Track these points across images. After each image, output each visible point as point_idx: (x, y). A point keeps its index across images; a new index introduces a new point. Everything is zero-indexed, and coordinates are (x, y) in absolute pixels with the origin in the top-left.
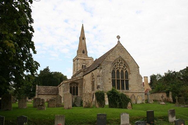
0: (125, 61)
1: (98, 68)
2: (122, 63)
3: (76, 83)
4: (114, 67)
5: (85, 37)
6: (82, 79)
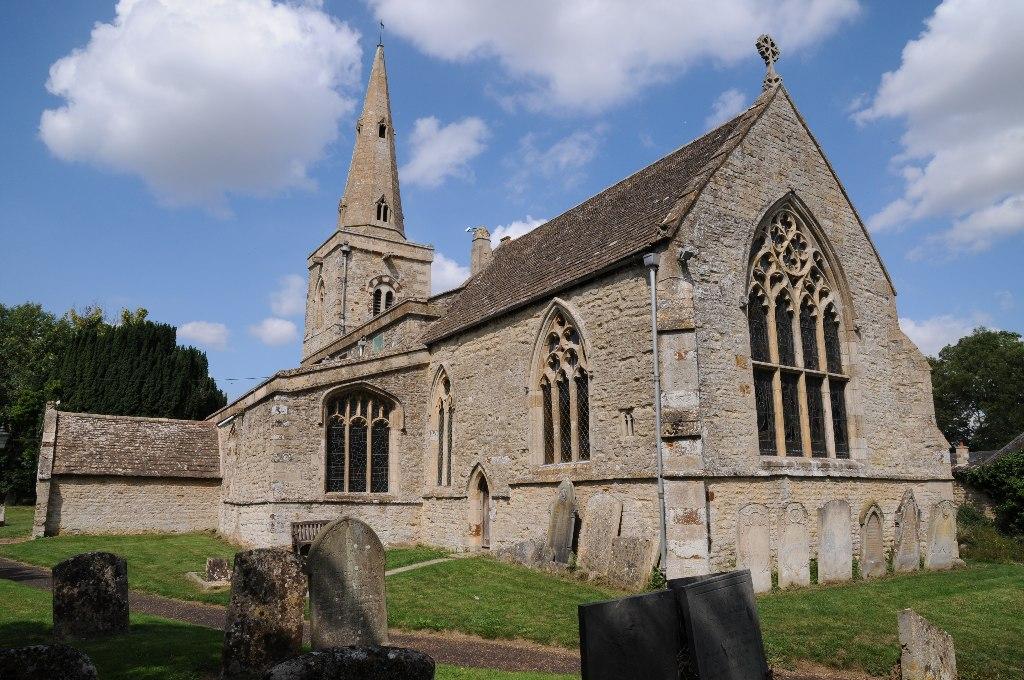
2: (800, 245)
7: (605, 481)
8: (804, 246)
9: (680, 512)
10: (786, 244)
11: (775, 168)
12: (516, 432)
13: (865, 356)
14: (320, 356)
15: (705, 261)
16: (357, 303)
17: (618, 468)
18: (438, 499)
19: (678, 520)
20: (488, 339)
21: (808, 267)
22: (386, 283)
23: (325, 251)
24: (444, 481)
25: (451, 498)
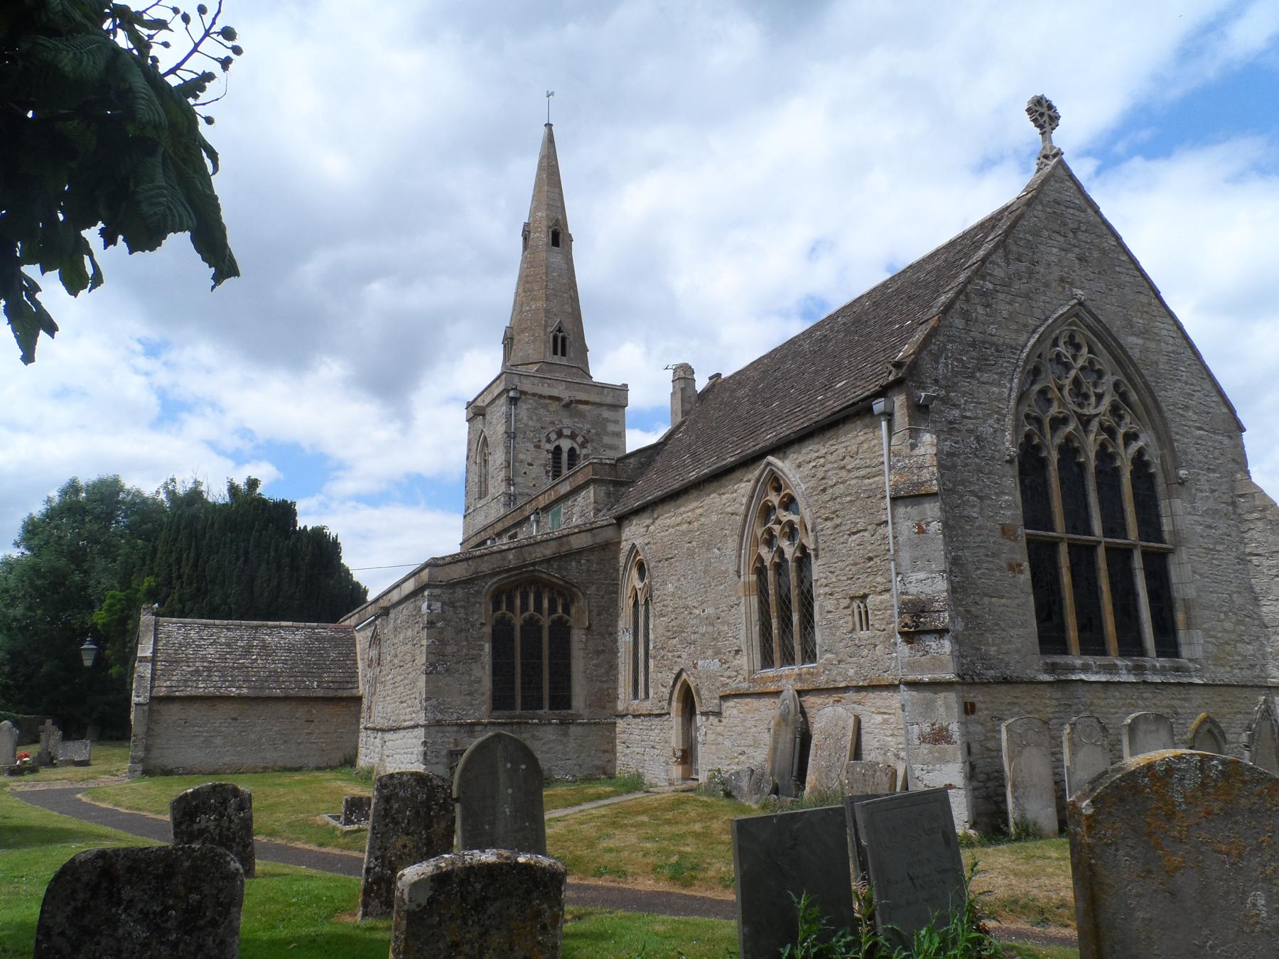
0: (1122, 359)
1: (879, 406)
3: (549, 585)
4: (1036, 412)
5: (572, 229)
6: (611, 547)
7: (837, 690)
8: (1100, 374)
9: (926, 728)
10: (1073, 373)
11: (1056, 273)
12: (726, 628)
13: (1196, 518)
14: (483, 536)
15: (954, 405)
16: (530, 464)
17: (851, 672)
18: (634, 716)
19: (923, 739)
20: (691, 509)
21: (1106, 401)
22: (567, 437)
23: (488, 399)
24: (641, 694)
25: (650, 715)
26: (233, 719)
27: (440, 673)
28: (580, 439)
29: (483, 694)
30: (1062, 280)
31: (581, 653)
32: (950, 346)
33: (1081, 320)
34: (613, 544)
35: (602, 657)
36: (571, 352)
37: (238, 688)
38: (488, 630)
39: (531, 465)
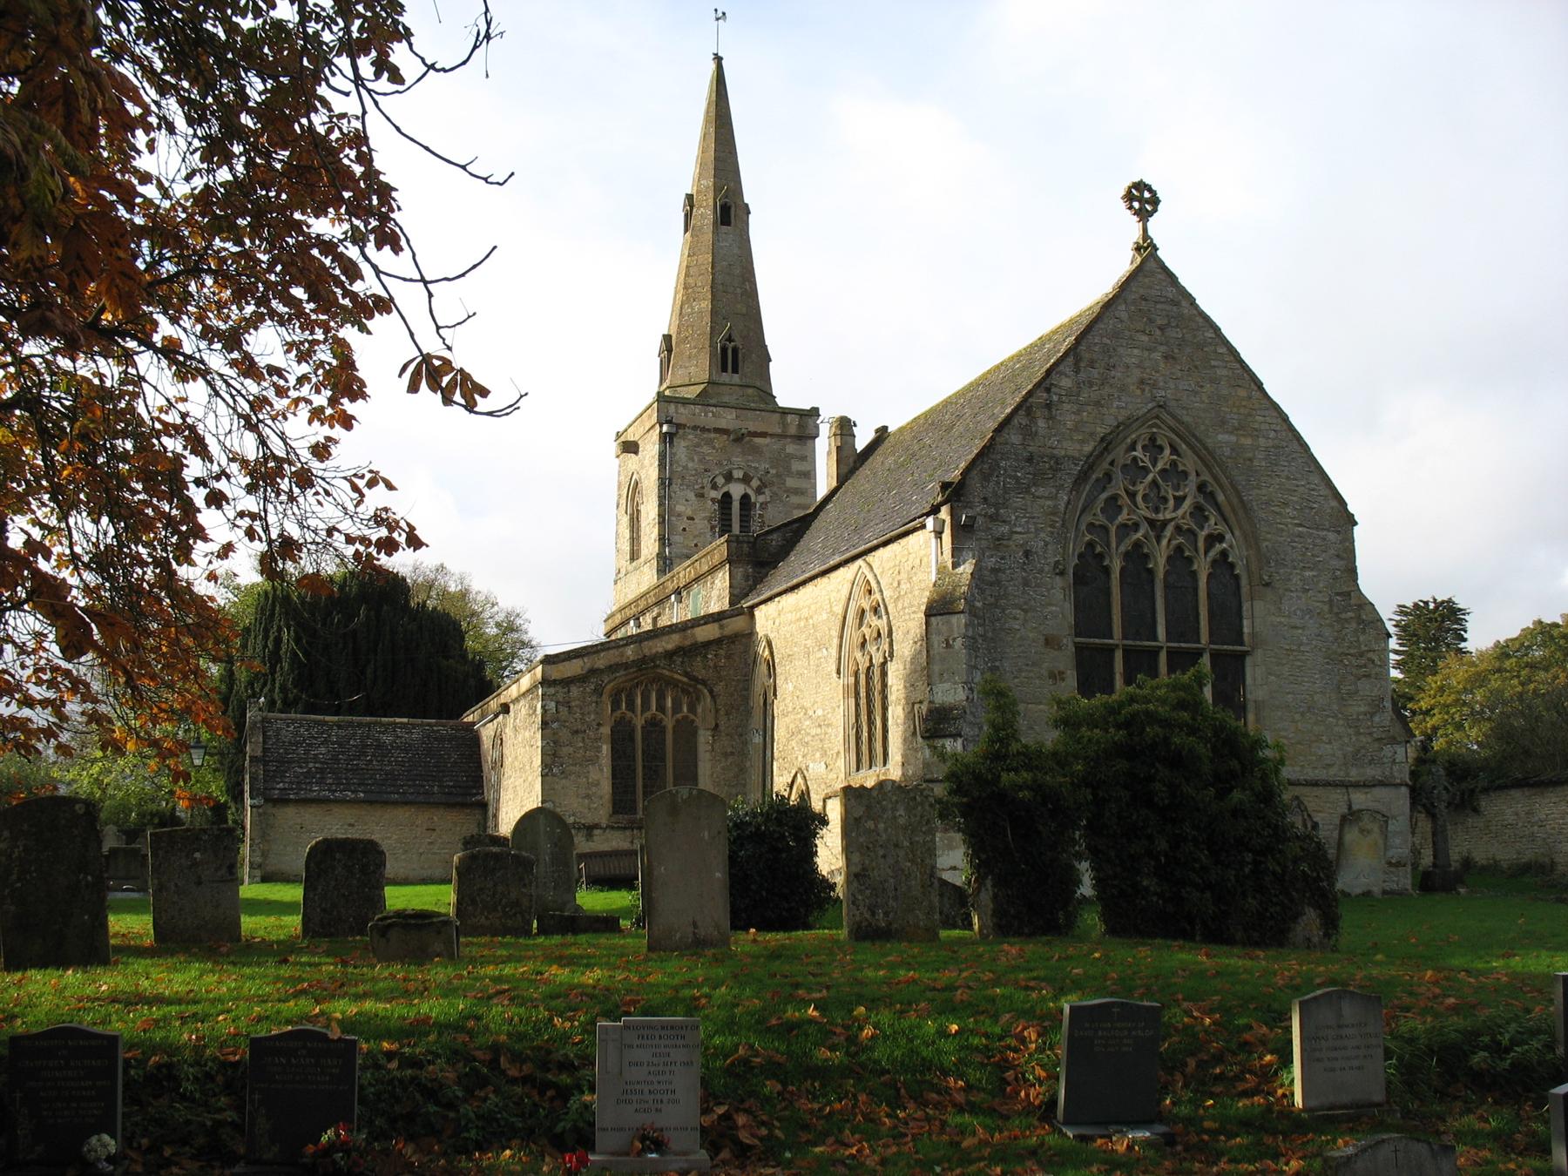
0: (1207, 457)
4: (1101, 519)
14: (629, 612)
21: (1187, 504)
26: (350, 825)
27: (554, 775)
28: (755, 483)
29: (601, 798)
30: (1142, 381)
31: (708, 755)
32: (1003, 464)
33: (1163, 422)
34: (743, 636)
35: (730, 759)
36: (746, 367)
37: (353, 792)
38: (606, 730)
39: (692, 519)
